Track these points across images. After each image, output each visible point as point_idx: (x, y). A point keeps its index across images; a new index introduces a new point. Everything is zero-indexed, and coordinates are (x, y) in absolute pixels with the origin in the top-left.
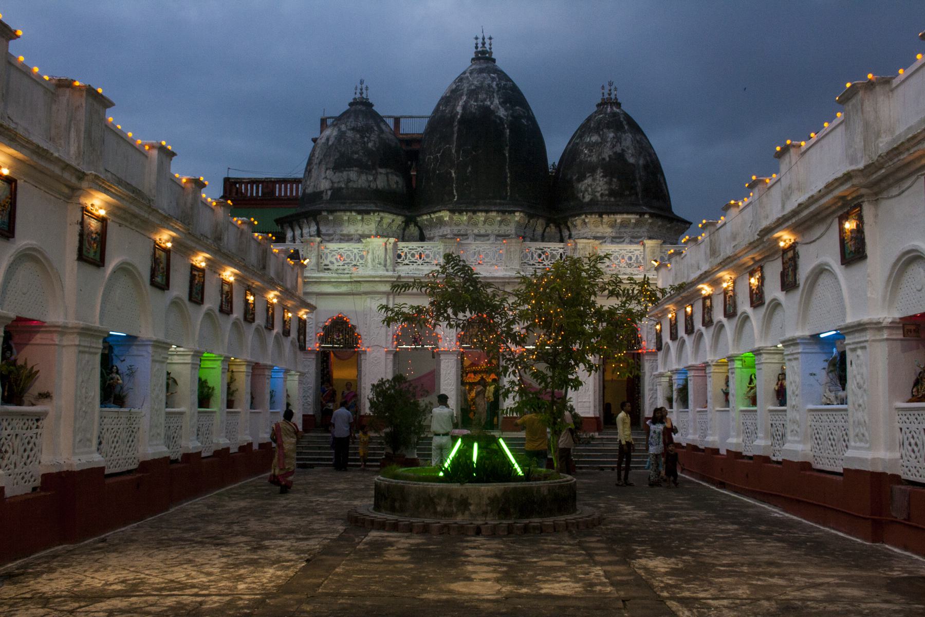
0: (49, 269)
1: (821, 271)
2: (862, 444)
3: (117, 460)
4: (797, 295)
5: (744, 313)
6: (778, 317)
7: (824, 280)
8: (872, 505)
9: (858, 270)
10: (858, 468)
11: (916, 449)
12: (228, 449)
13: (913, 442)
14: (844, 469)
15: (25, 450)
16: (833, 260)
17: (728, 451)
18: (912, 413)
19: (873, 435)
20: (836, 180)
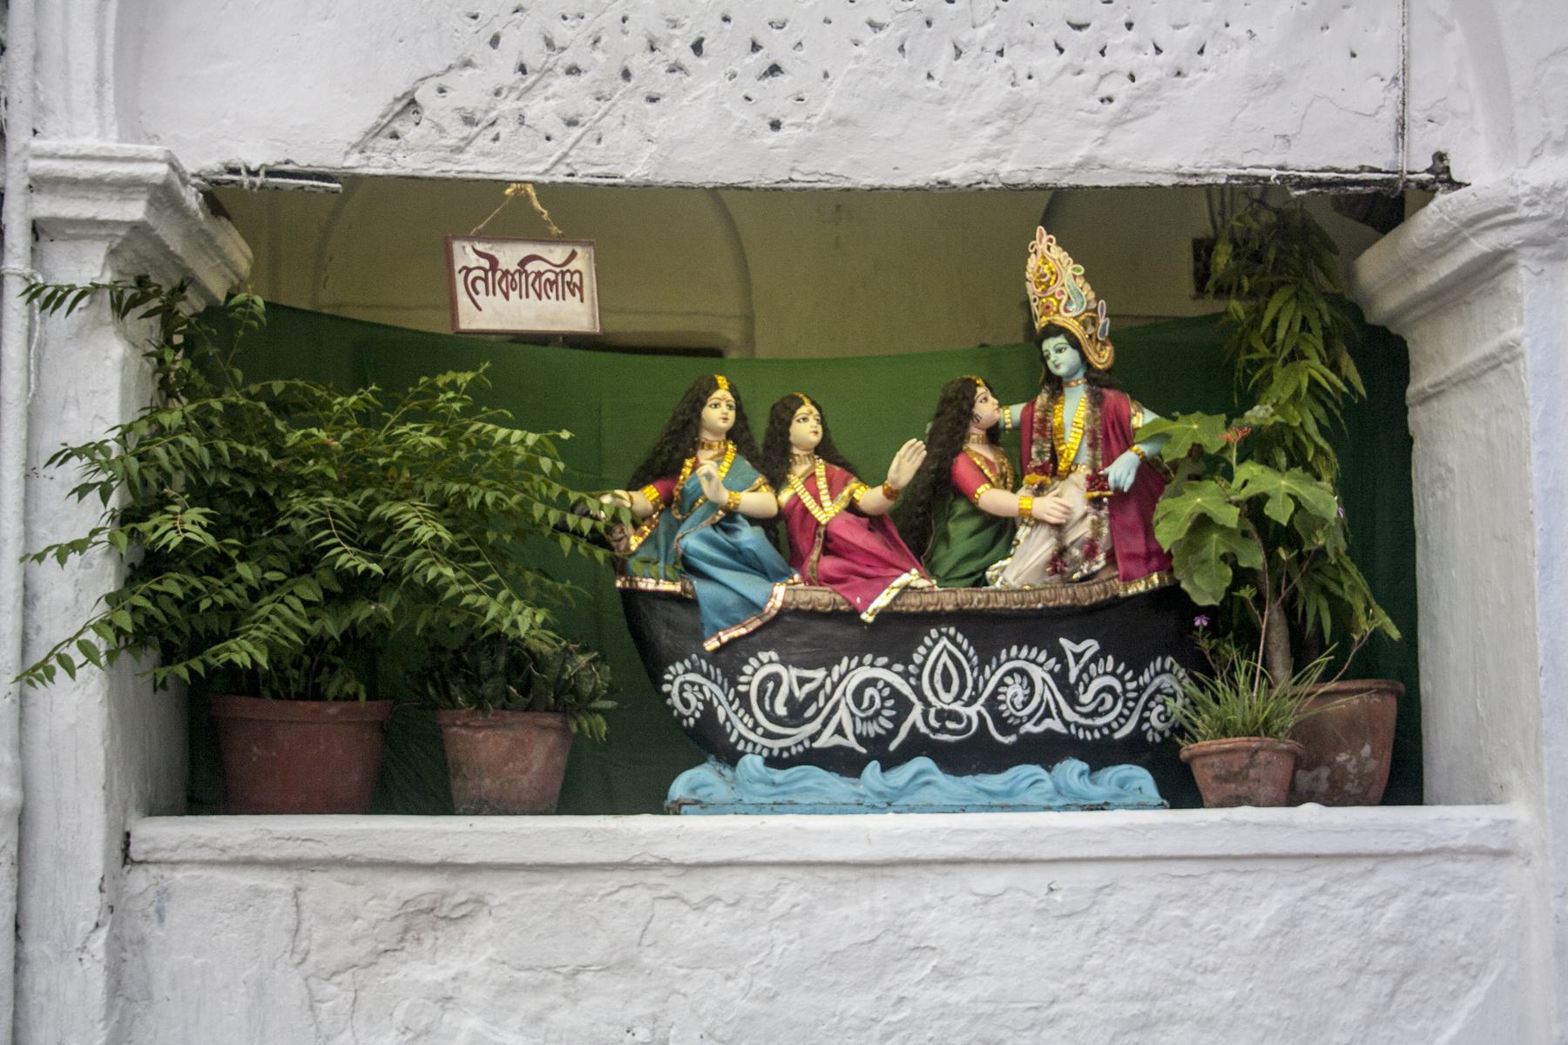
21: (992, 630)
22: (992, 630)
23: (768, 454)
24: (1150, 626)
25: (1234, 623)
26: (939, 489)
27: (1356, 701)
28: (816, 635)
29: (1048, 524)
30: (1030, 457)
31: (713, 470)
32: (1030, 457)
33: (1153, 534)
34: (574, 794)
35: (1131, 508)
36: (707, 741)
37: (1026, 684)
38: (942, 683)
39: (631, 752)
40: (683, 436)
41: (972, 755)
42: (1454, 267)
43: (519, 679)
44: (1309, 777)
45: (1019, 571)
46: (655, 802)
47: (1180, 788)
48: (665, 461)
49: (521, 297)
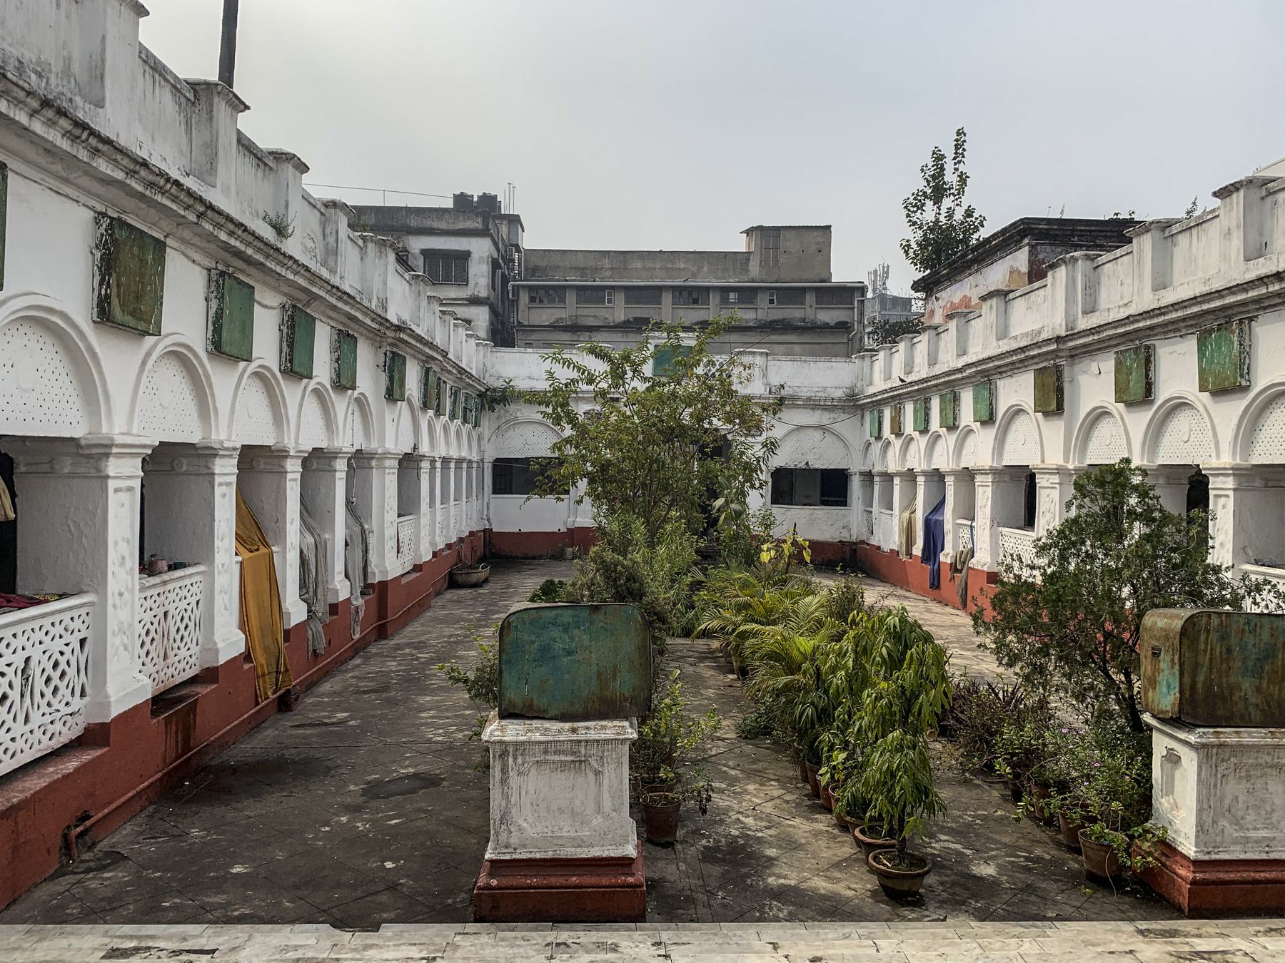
6: (970, 441)
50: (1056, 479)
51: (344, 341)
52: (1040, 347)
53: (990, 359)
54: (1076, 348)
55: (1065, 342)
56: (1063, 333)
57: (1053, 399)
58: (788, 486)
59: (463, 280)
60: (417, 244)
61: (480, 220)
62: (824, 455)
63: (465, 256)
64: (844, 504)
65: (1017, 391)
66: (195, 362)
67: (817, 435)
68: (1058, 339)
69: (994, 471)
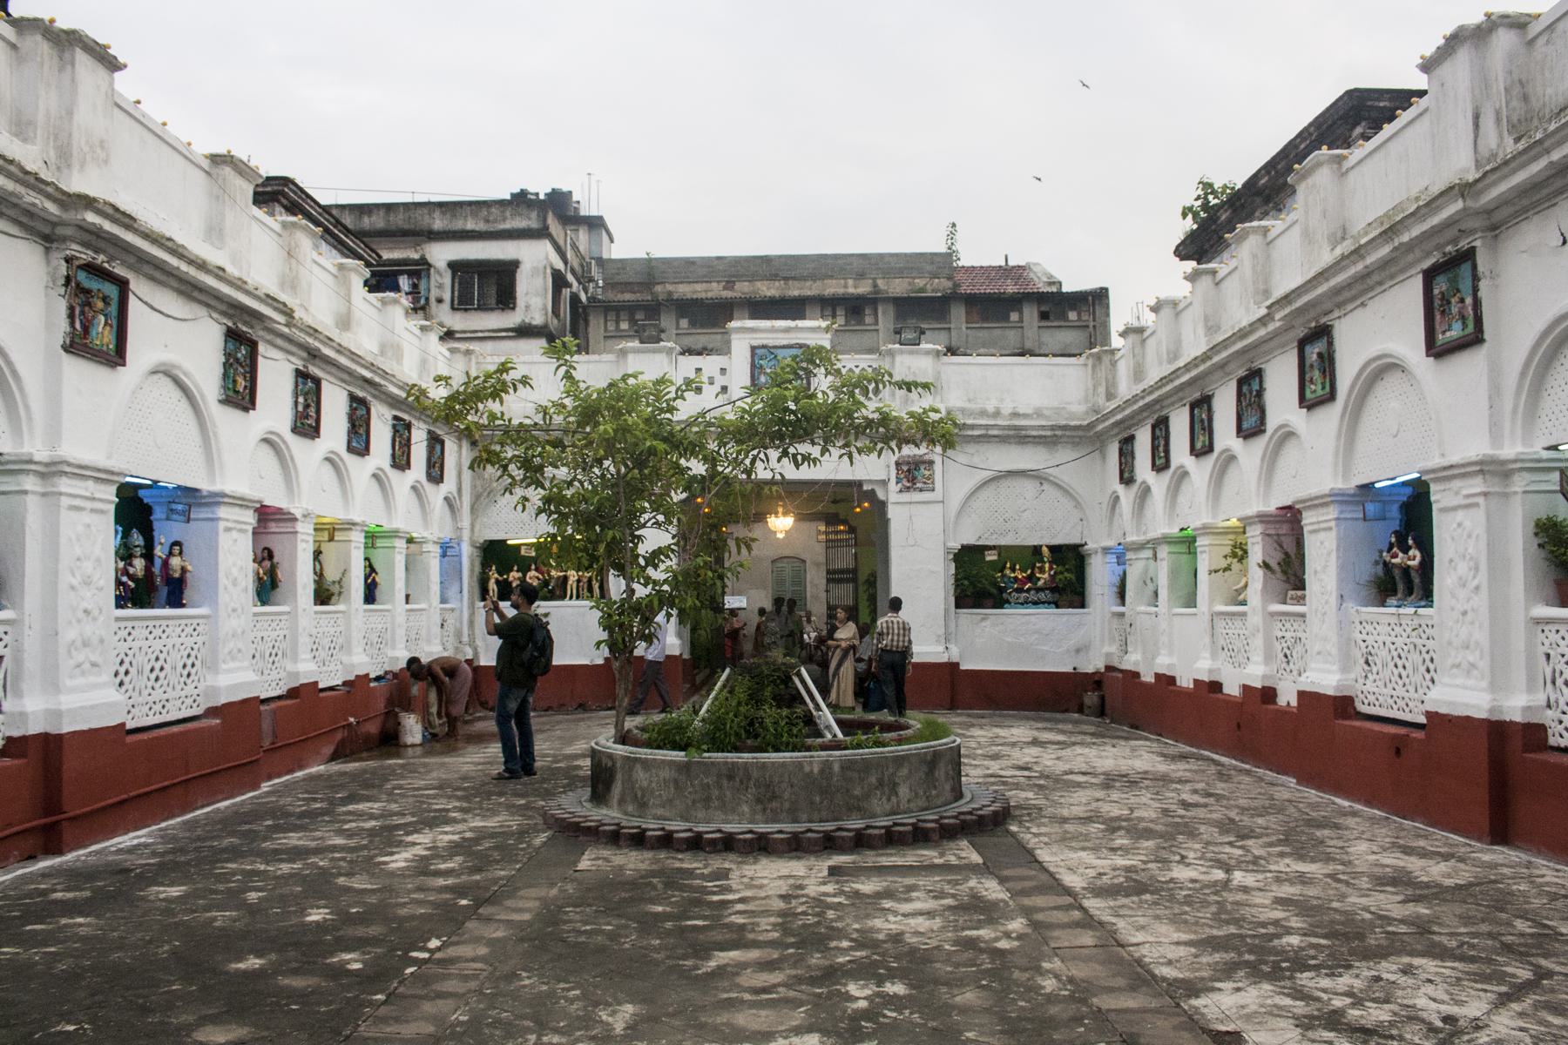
0: (25, 428)
1: (1383, 369)
2: (237, 664)
3: (173, 702)
4: (1330, 416)
5: (1227, 450)
6: (1290, 453)
7: (1392, 382)
8: (1494, 779)
9: (1470, 364)
10: (245, 696)
11: (1404, 674)
12: (1269, 694)
13: (1400, 663)
14: (1428, 714)
15: (152, 670)
16: (1407, 342)
17: (1196, 681)
18: (157, 623)
19: (1467, 658)
20: (285, 304)
21: (1038, 590)
22: (1038, 590)
23: (1013, 570)
24: (1053, 590)
25: (1064, 589)
26: (1033, 573)
27: (1076, 598)
28: (1019, 590)
29: (1043, 578)
30: (1042, 570)
31: (1008, 572)
32: (1042, 570)
33: (536, 327)
34: (994, 607)
35: (1052, 577)
36: (1008, 602)
37: (1042, 596)
38: (1033, 596)
39: (1000, 603)
40: (1004, 567)
41: (1035, 603)
42: (1520, 553)
43: (990, 594)
44: (1071, 606)
45: (1040, 583)
46: (803, 317)
47: (1057, 607)
48: (1002, 571)
49: (991, 557)
50: (1476, 485)
51: (308, 388)
52: (1423, 219)
53: (1322, 276)
54: (1503, 202)
55: (1480, 193)
56: (1471, 176)
57: (1454, 324)
58: (980, 580)
59: (506, 299)
60: (441, 254)
61: (534, 215)
62: (1031, 520)
63: (513, 266)
64: (1083, 606)
65: (1386, 327)
66: (14, 388)
67: (1028, 488)
68: (1464, 189)
69: (1338, 498)
